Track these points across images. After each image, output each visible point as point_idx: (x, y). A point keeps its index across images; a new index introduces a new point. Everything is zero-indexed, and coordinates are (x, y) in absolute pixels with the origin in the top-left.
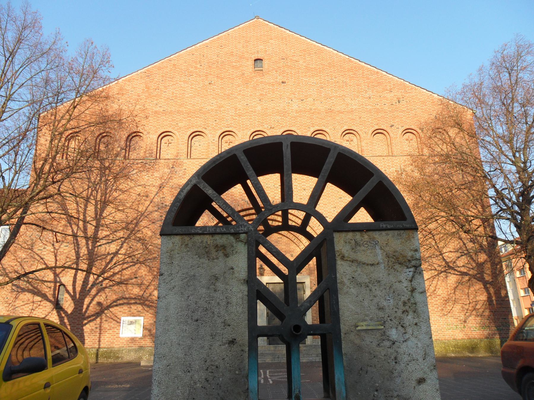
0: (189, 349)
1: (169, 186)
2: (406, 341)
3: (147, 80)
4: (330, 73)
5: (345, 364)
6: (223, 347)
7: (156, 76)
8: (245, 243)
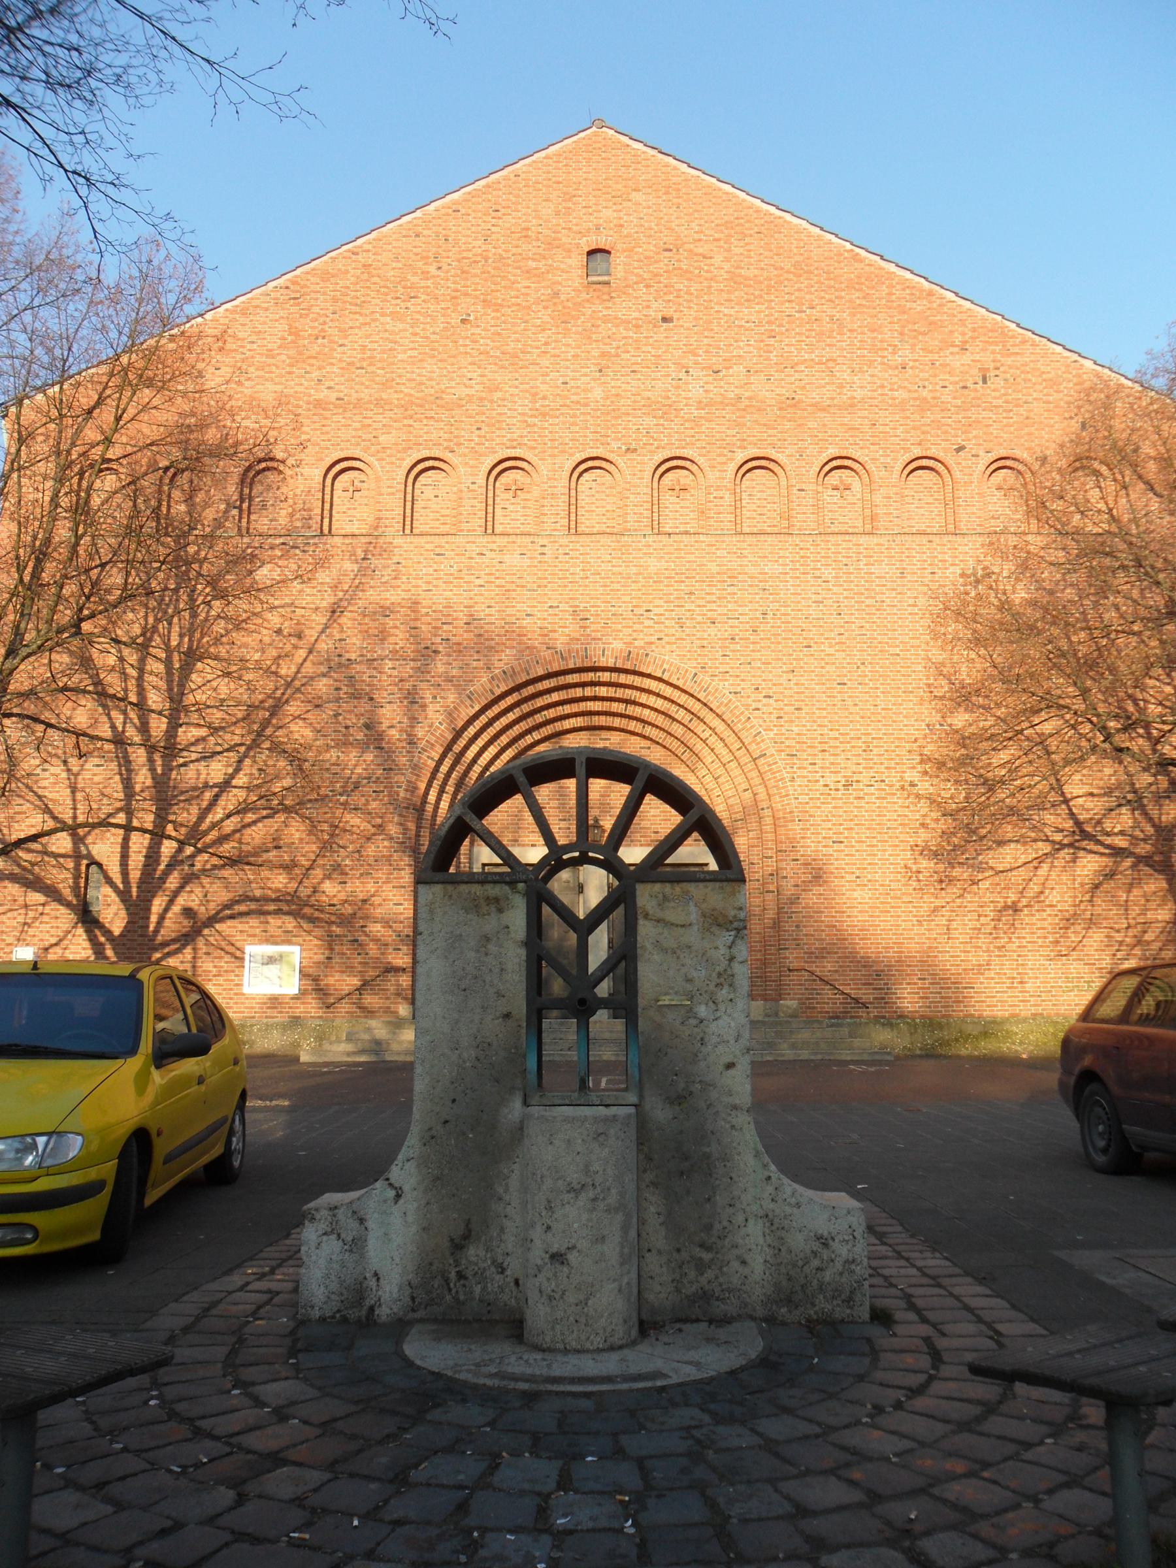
1: (355, 608)
3: (293, 309)
4: (797, 294)
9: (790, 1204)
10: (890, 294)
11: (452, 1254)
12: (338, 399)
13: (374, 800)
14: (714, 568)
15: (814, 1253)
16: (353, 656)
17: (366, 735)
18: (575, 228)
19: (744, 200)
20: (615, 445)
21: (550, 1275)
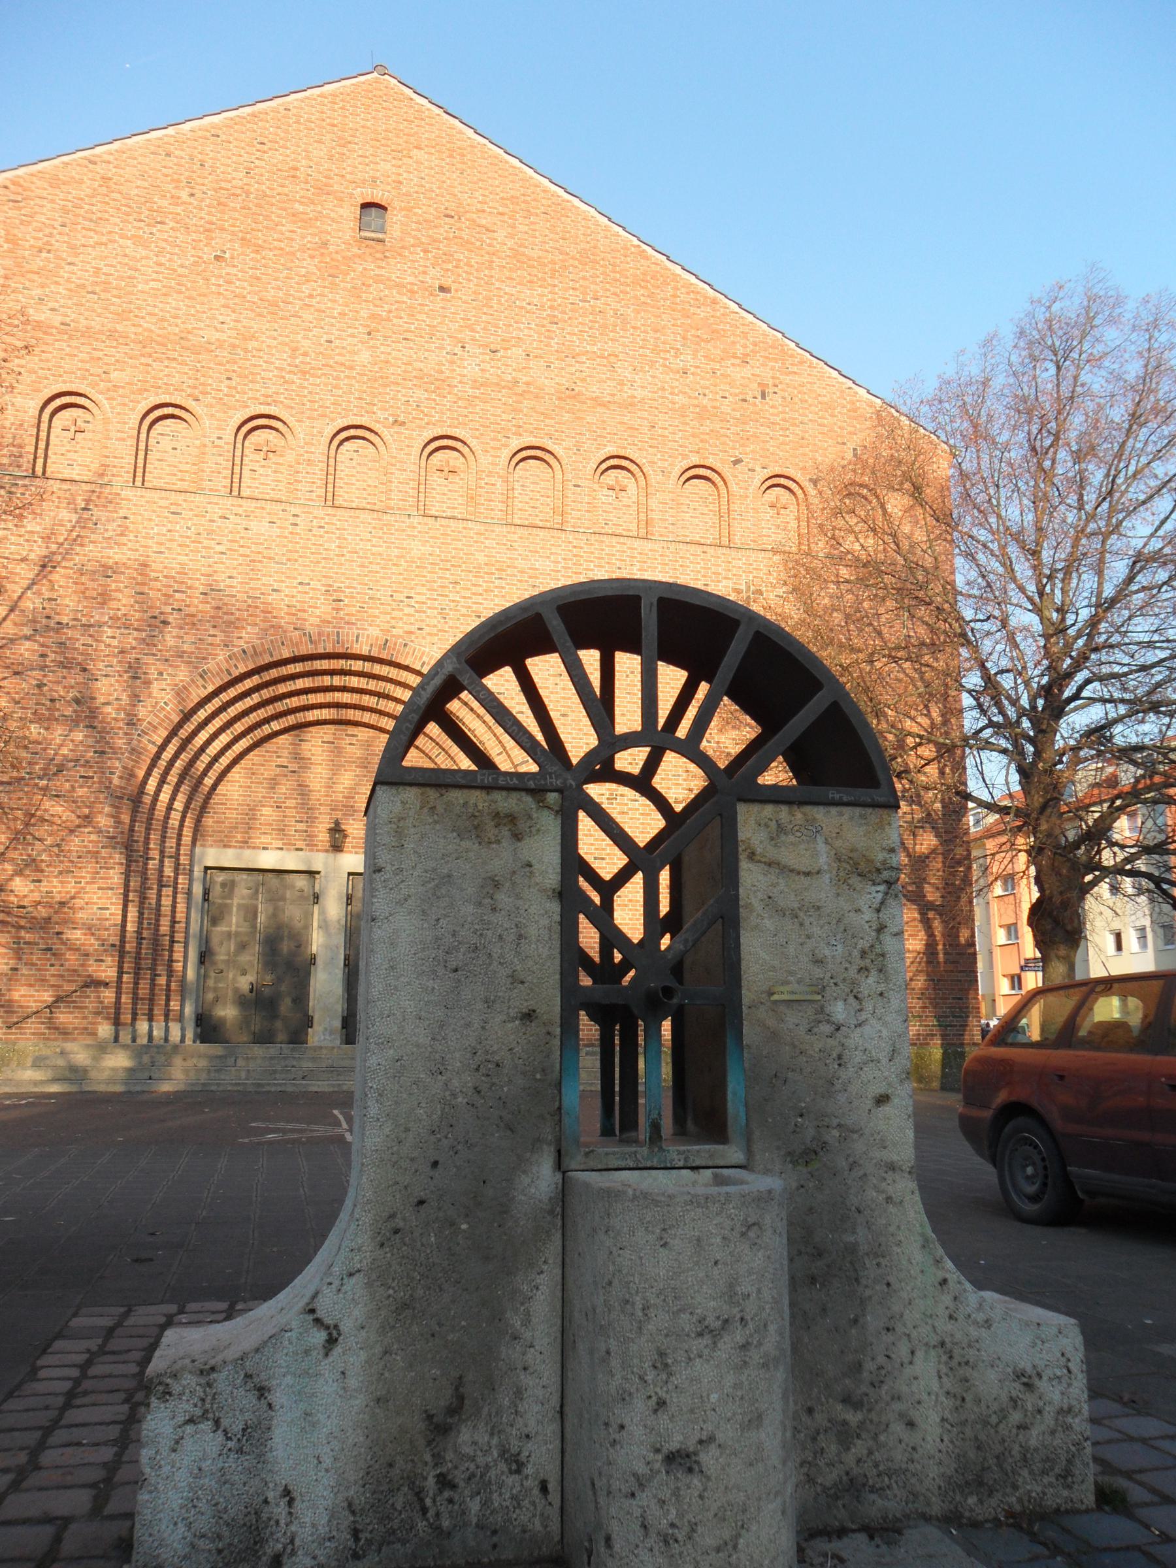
0: (441, 1027)
1: (71, 564)
2: (860, 1025)
3: (11, 213)
4: (581, 282)
5: (747, 1065)
6: (510, 1025)
7: (42, 206)
8: (557, 812)
9: (976, 1323)
10: (674, 296)
11: (429, 1443)
12: (63, 324)
13: (81, 787)
14: (481, 558)
15: (1014, 1401)
16: (65, 620)
17: (75, 711)
18: (348, 177)
19: (531, 178)
20: (381, 415)
21: (666, 1493)
